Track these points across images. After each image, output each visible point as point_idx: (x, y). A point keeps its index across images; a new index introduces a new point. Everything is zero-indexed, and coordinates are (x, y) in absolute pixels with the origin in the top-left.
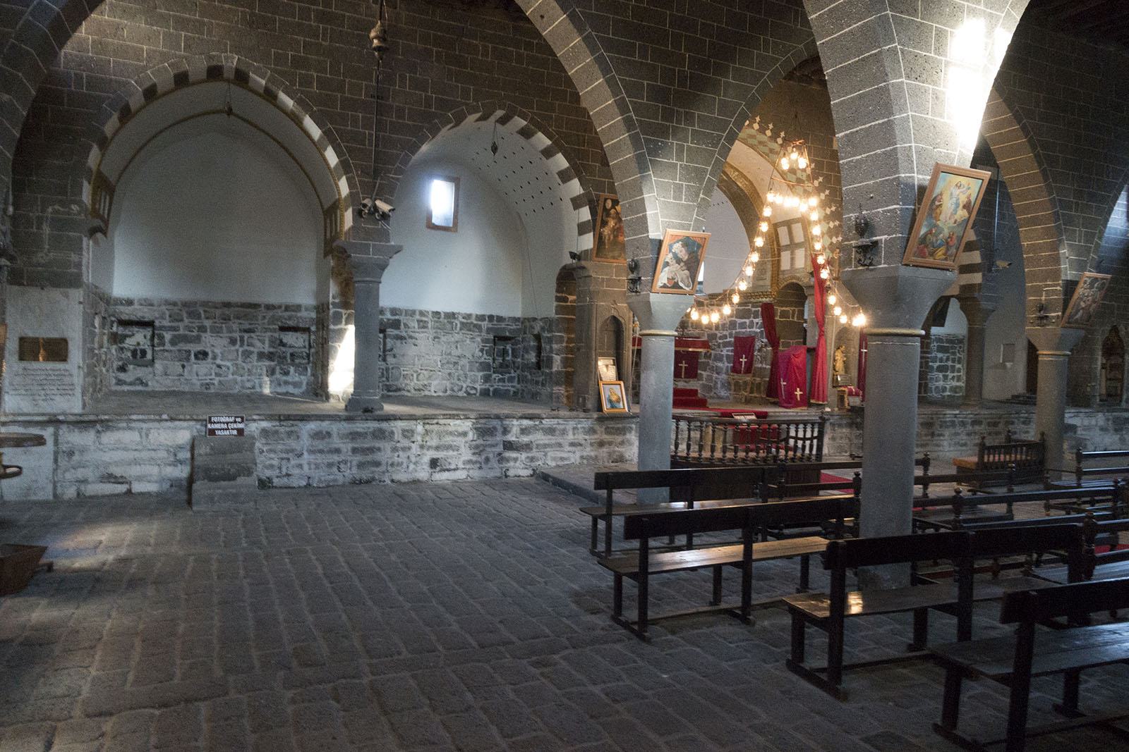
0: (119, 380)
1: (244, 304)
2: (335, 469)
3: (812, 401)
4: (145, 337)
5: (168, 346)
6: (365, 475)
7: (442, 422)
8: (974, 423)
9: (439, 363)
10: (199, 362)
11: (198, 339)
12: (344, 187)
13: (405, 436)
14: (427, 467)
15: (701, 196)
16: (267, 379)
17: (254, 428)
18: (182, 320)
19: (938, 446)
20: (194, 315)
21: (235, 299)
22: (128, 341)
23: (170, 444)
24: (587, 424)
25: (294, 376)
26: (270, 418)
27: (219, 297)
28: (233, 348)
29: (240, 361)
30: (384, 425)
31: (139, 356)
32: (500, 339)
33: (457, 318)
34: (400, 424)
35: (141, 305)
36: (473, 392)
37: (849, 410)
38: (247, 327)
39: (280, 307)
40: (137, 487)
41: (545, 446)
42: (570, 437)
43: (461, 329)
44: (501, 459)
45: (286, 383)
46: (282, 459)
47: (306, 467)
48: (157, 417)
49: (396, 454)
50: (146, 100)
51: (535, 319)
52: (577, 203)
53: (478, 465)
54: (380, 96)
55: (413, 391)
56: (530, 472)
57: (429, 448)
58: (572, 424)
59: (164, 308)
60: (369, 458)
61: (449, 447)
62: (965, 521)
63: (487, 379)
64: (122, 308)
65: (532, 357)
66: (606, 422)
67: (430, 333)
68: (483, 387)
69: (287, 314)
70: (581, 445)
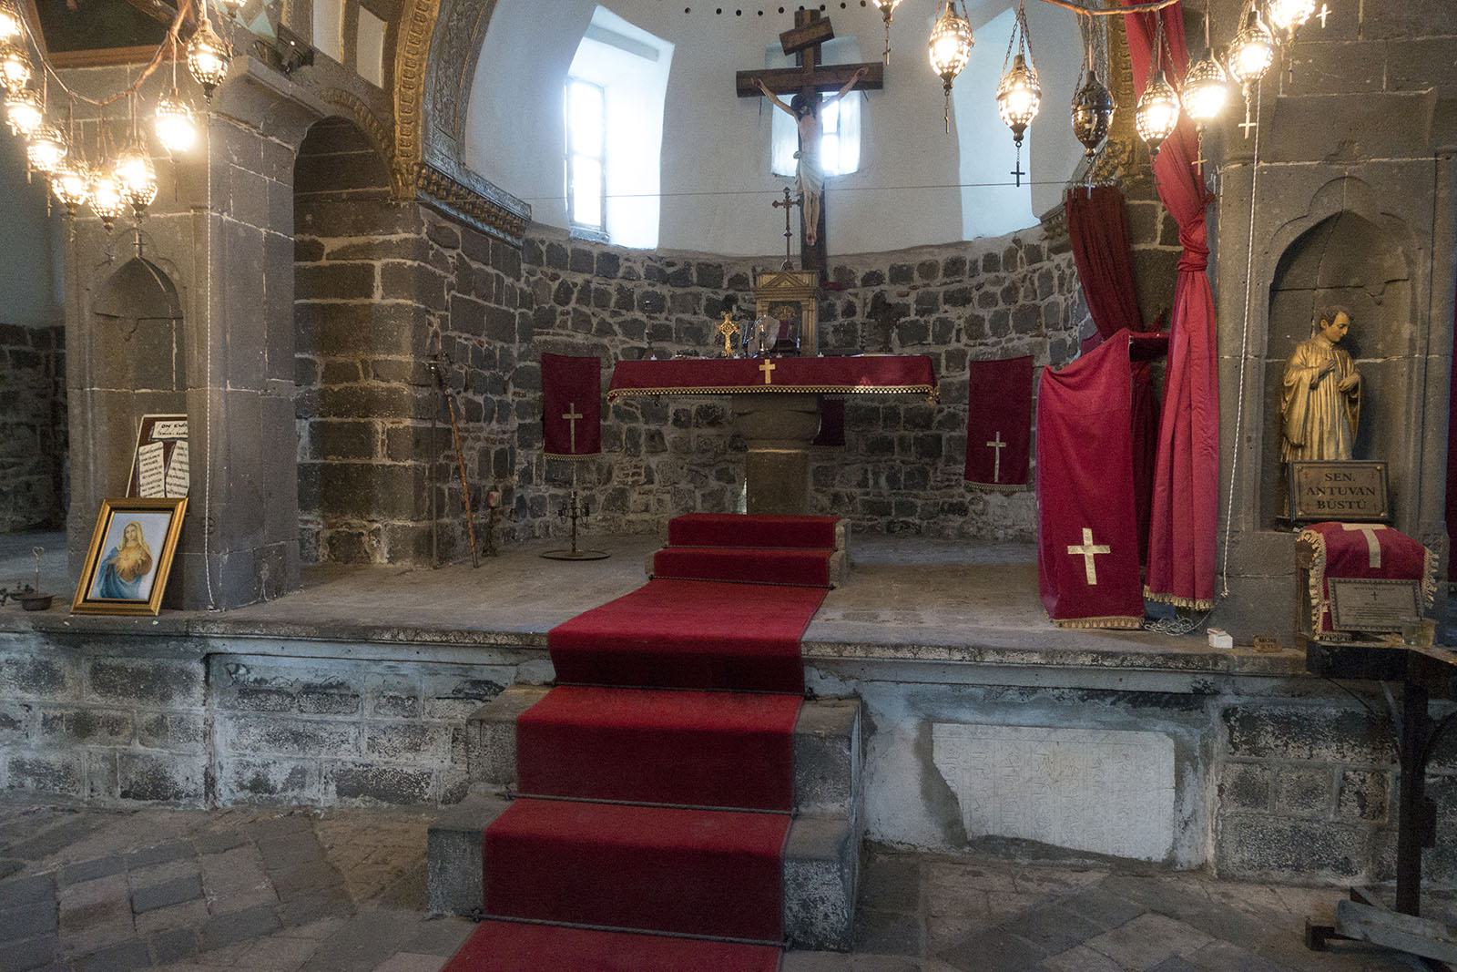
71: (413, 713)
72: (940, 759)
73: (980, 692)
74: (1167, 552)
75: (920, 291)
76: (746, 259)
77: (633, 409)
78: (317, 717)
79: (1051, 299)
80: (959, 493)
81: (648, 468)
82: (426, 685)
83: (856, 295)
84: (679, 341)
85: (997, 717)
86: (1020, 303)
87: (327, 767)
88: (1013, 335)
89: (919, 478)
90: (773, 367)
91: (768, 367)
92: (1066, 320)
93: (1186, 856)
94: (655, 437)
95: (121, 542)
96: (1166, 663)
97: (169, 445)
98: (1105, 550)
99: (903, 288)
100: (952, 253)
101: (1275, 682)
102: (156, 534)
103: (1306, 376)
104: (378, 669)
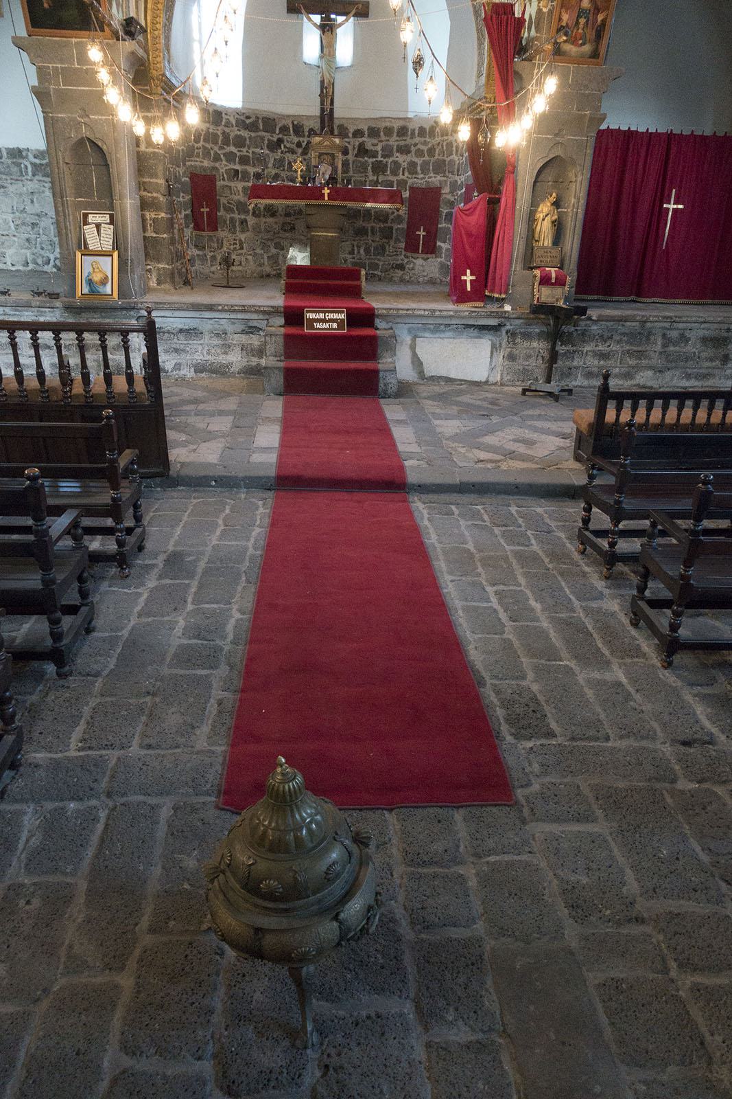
9: (11, 224)
33: (27, 157)
43: (34, 175)
62: (707, 532)
71: (225, 339)
72: (418, 350)
73: (432, 327)
74: (494, 279)
75: (384, 143)
76: (288, 116)
77: (232, 206)
78: (185, 342)
79: (451, 157)
80: (401, 259)
81: (240, 240)
83: (349, 143)
84: (254, 165)
85: (437, 335)
86: (436, 158)
87: (190, 362)
88: (432, 175)
89: (381, 250)
90: (329, 191)
91: (326, 191)
92: (458, 171)
93: (492, 380)
94: (244, 222)
95: (91, 270)
96: (490, 315)
97: (98, 226)
98: (474, 278)
99: (375, 141)
100: (401, 123)
101: (522, 321)
102: (107, 266)
103: (541, 216)
104: (211, 322)
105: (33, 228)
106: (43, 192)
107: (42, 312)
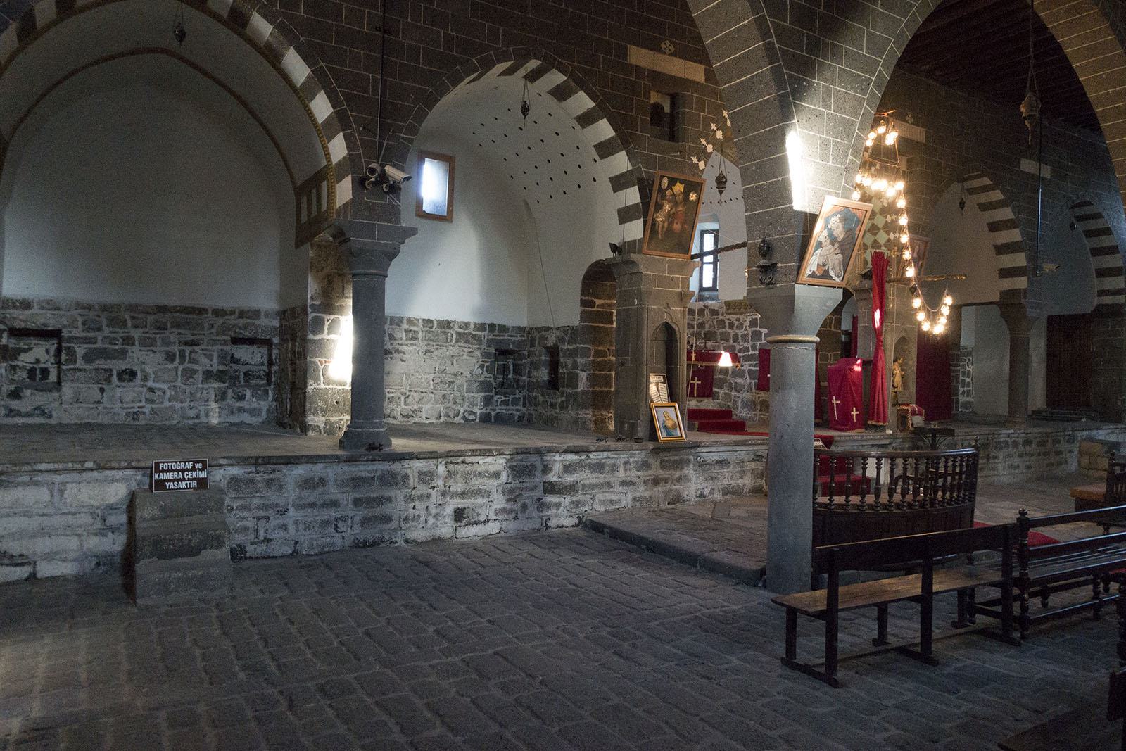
0: (11, 410)
1: (186, 308)
2: (331, 530)
3: (870, 422)
4: (47, 352)
5: (80, 364)
6: (370, 534)
7: (469, 460)
8: (1027, 442)
9: (431, 382)
10: (123, 384)
11: (122, 354)
12: (338, 148)
13: (422, 481)
14: (450, 520)
15: (850, 157)
16: (214, 405)
17: (219, 476)
18: (100, 329)
19: (993, 469)
20: (115, 322)
21: (172, 302)
22: (23, 357)
23: (96, 504)
24: (639, 457)
25: (251, 401)
26: (243, 461)
27: (150, 298)
28: (170, 366)
29: (179, 383)
30: (396, 467)
31: (37, 376)
32: (502, 353)
34: (417, 465)
35: (43, 308)
36: (472, 417)
37: (912, 432)
38: (190, 338)
39: (232, 312)
40: (45, 570)
41: (593, 486)
42: (621, 474)
43: (456, 342)
44: (541, 505)
45: (241, 410)
46: (259, 518)
47: (292, 528)
48: (79, 466)
49: (412, 505)
50: (59, 13)
51: (548, 329)
52: (619, 183)
53: (514, 515)
54: (385, 29)
55: (400, 417)
56: (574, 521)
57: (454, 495)
58: (623, 457)
59: (75, 312)
60: (376, 511)
61: (478, 493)
63: (487, 401)
64: (15, 313)
65: (543, 374)
66: (661, 454)
67: (421, 345)
68: (484, 411)
69: (242, 322)
70: (633, 484)
82: (746, 458)
95: (664, 418)
98: (858, 413)
105: (449, 386)
106: (463, 355)
107: (633, 454)
